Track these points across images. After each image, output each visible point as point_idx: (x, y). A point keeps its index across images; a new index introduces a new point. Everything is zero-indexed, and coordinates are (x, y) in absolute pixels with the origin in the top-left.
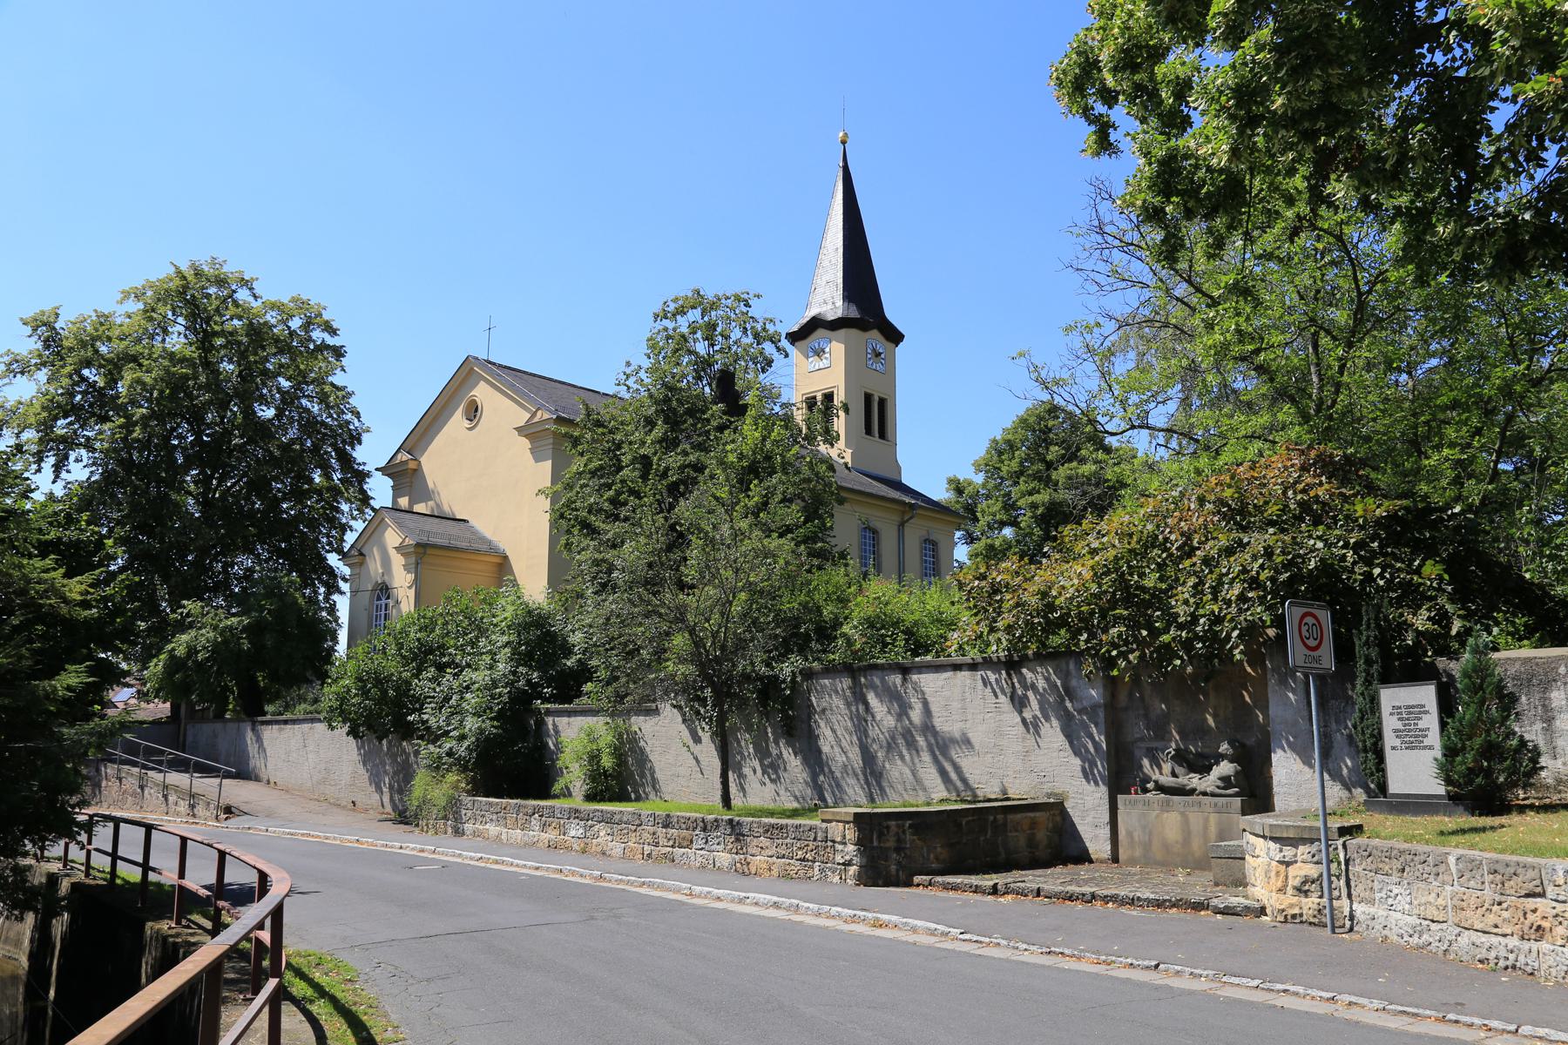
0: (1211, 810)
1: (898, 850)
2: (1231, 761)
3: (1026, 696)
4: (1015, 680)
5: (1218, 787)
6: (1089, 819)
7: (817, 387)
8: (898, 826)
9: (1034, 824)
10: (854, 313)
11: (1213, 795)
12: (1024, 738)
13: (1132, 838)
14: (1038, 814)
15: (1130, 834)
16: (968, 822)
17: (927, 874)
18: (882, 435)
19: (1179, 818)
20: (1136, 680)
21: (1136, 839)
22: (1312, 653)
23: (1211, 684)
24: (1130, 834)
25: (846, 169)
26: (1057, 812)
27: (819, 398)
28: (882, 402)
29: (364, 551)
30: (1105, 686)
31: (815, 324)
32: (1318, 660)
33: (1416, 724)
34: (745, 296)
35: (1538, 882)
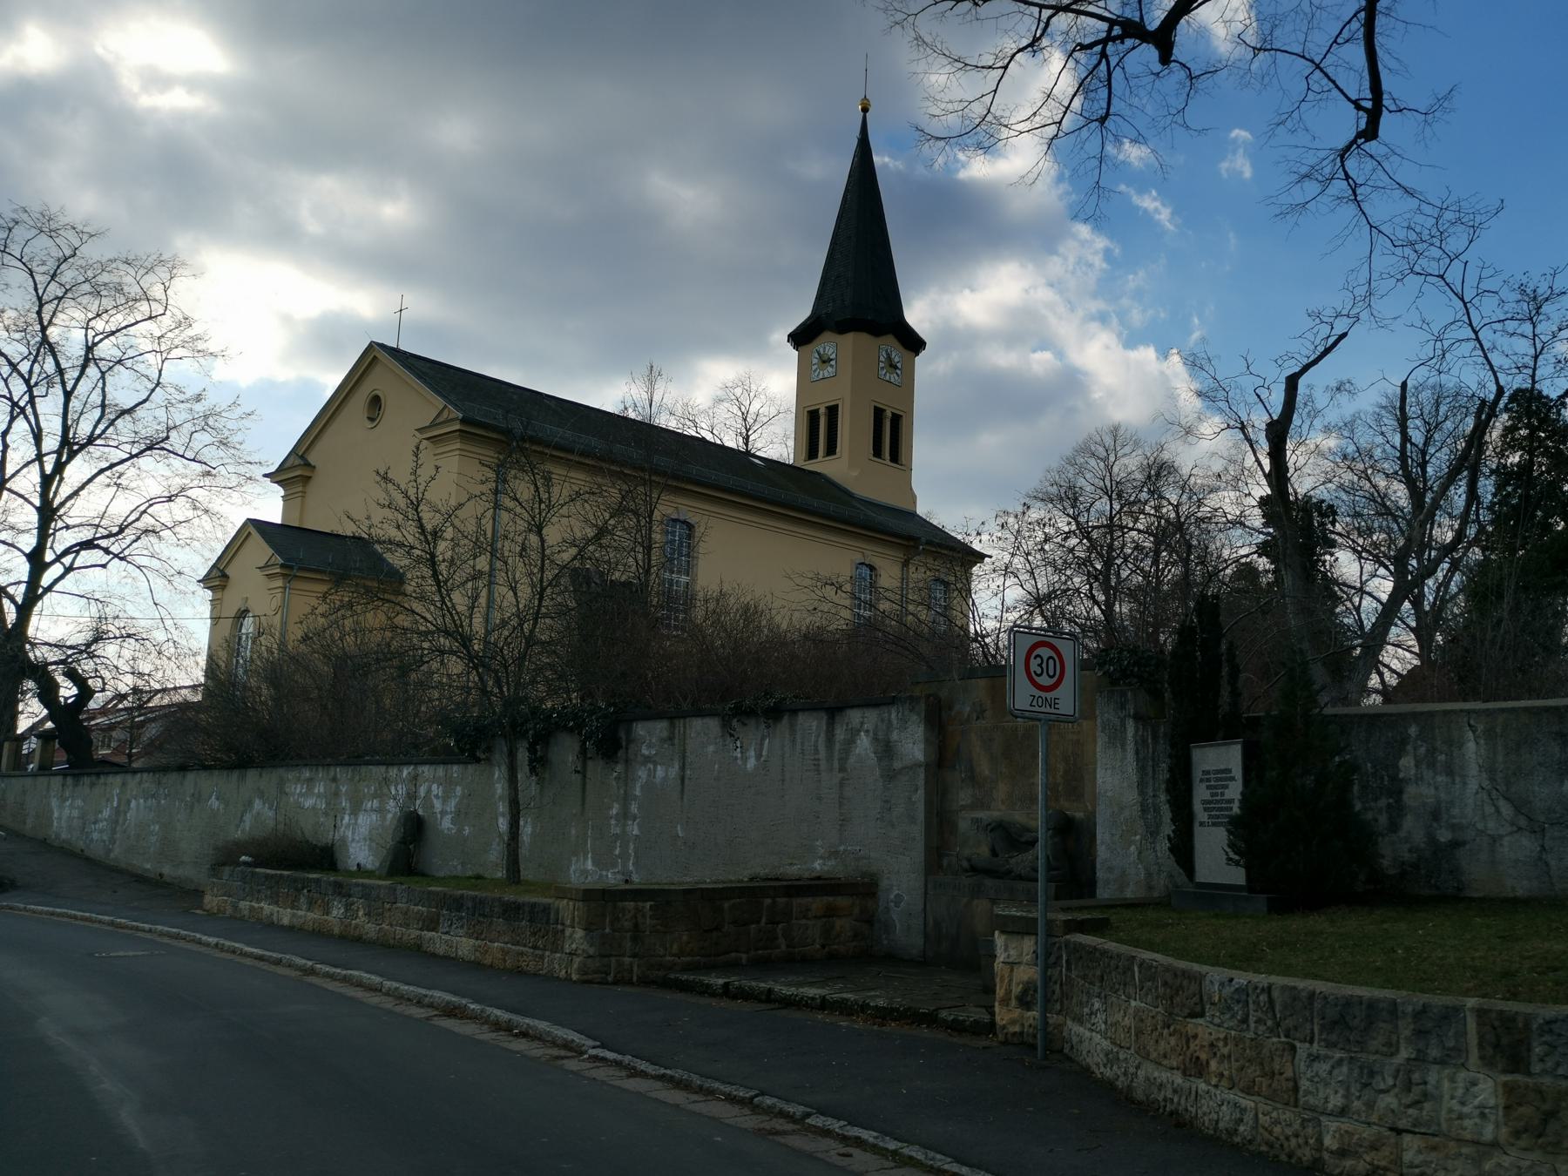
17: (381, 976)
18: (895, 458)
22: (1043, 694)
27: (822, 411)
28: (896, 419)
29: (227, 572)
32: (1054, 703)
33: (1222, 794)
35: (1196, 999)
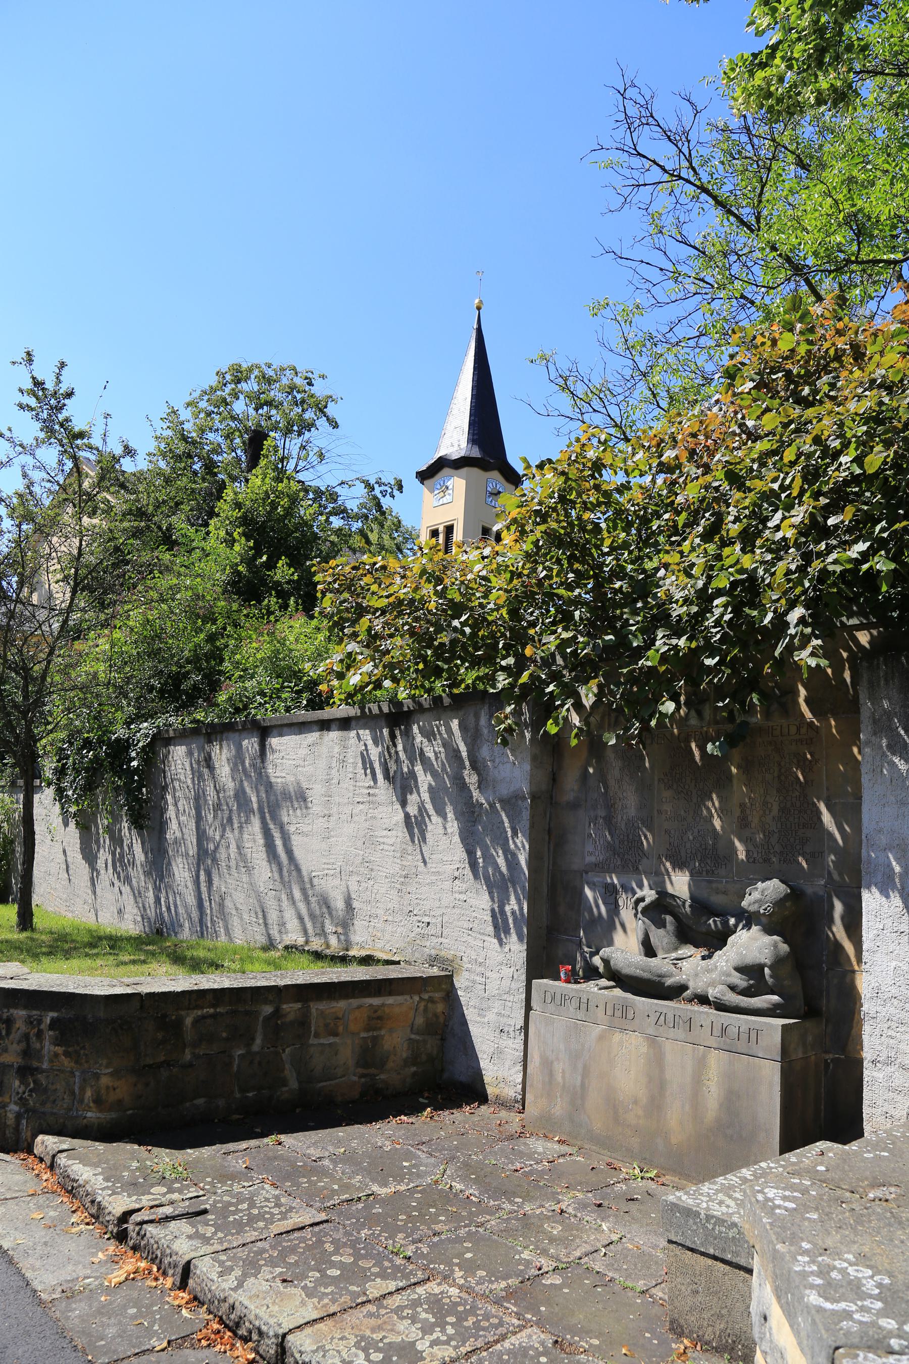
0: (712, 1042)
1: (25, 1072)
2: (769, 930)
3: (412, 775)
4: (400, 747)
5: (733, 988)
6: (491, 1016)
7: (439, 520)
8: (29, 1021)
9: (376, 1020)
10: (476, 453)
11: (721, 1007)
12: (404, 852)
13: (551, 1074)
14: (390, 1000)
15: (547, 1065)
16: (197, 1021)
19: (644, 1049)
20: (595, 746)
21: (559, 1078)
23: (736, 753)
24: (547, 1065)
25: (479, 331)
26: (437, 995)
30: (535, 760)
31: (440, 465)
34: (310, 375)
